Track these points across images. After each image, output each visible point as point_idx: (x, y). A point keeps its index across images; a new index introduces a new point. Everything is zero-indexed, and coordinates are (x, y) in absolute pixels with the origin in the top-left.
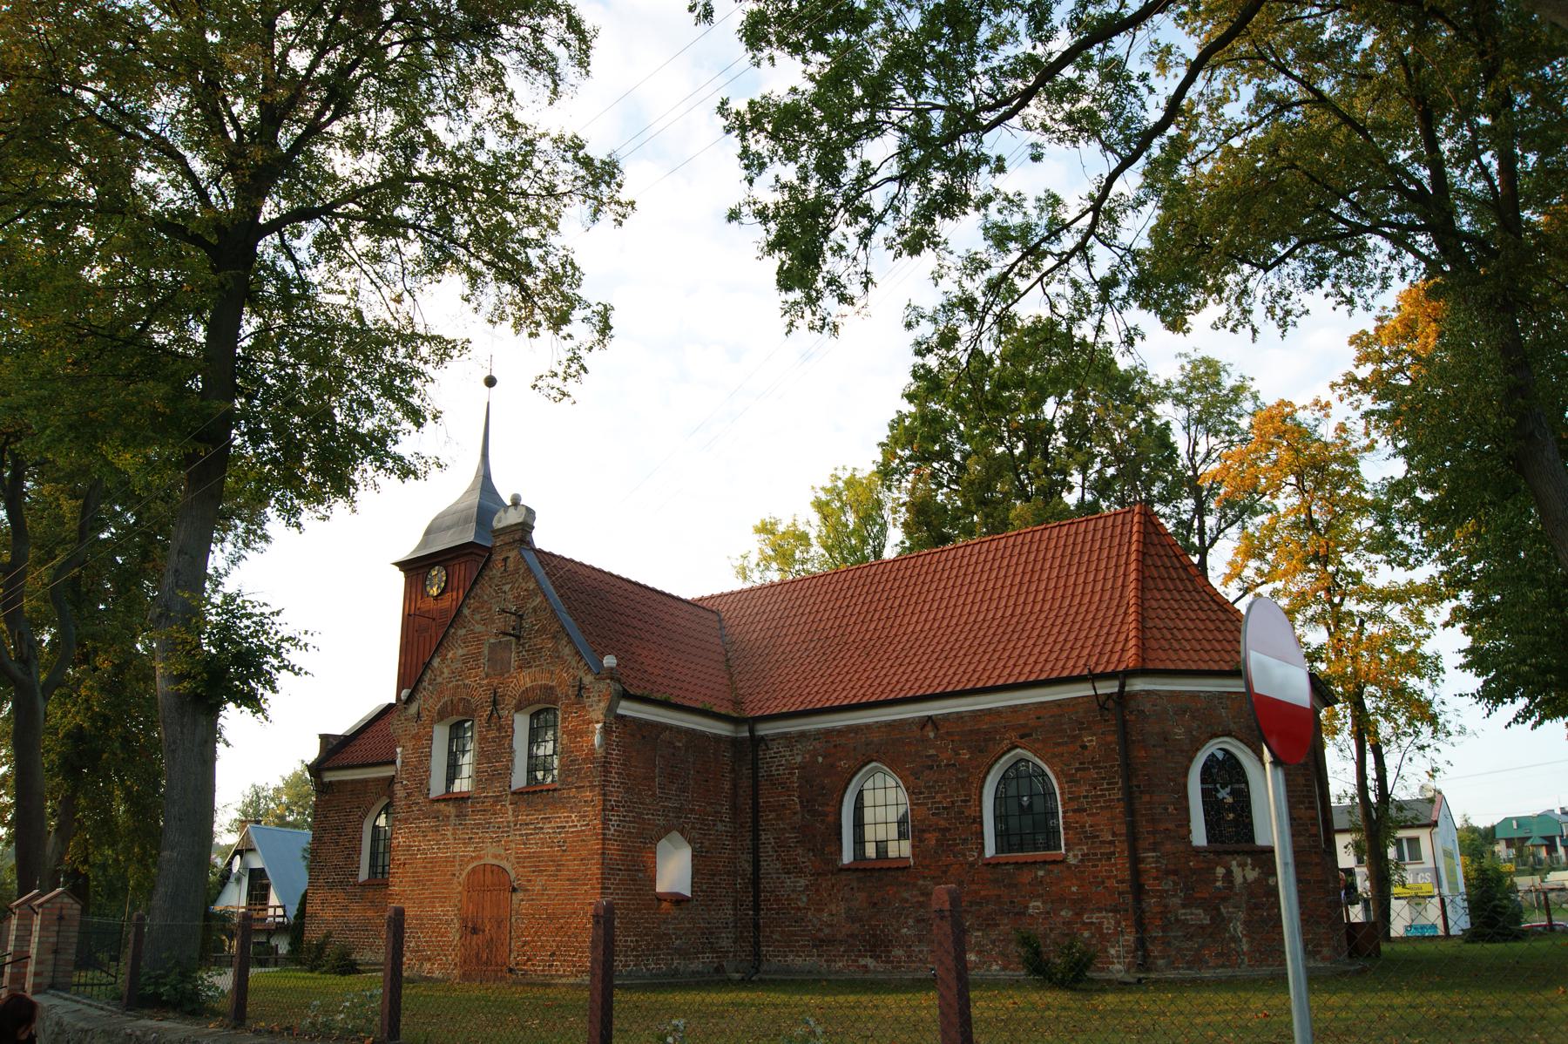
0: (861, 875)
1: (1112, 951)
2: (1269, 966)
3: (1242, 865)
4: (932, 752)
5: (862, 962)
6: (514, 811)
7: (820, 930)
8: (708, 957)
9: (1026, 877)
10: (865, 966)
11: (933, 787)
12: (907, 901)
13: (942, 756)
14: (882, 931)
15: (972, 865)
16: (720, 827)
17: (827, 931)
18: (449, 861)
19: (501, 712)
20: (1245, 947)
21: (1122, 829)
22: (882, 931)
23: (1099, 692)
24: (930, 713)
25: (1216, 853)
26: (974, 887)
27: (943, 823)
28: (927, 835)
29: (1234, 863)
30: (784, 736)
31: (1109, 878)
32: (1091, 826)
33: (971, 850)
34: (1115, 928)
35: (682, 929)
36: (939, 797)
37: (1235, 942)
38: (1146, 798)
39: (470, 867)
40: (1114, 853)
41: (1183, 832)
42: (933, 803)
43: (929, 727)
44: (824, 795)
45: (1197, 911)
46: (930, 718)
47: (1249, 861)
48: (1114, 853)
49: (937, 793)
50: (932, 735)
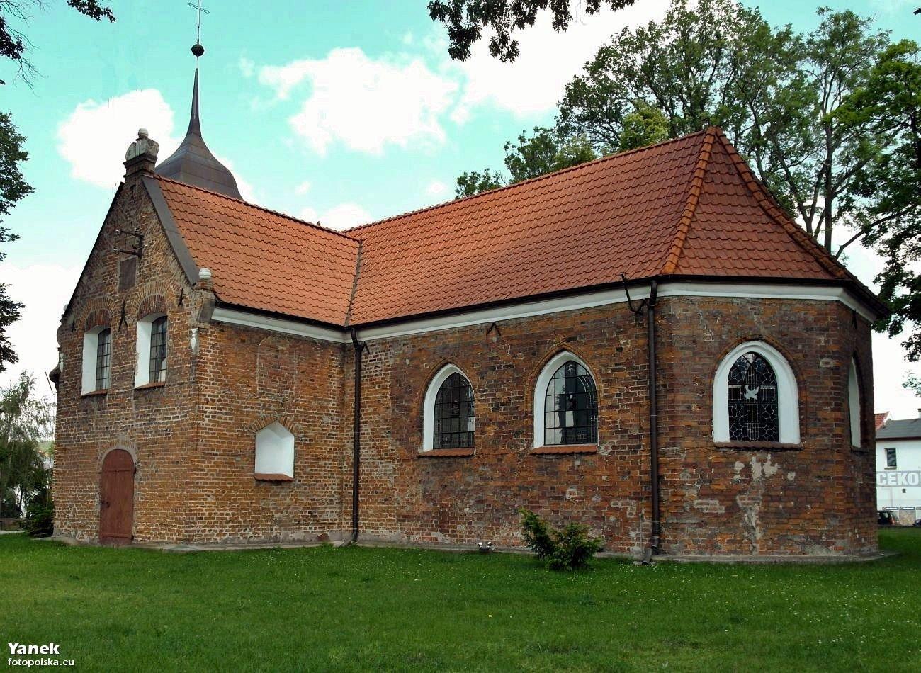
0: (435, 461)
1: (633, 534)
2: (780, 553)
3: (762, 461)
4: (495, 354)
5: (434, 534)
6: (137, 405)
7: (403, 507)
8: (311, 527)
9: (565, 466)
10: (436, 539)
11: (494, 386)
12: (469, 484)
13: (503, 358)
14: (450, 509)
15: (522, 454)
16: (326, 419)
17: (408, 508)
18: (94, 446)
19: (127, 321)
20: (758, 535)
21: (645, 424)
22: (450, 509)
23: (632, 298)
24: (494, 320)
25: (737, 449)
26: (524, 474)
27: (501, 418)
28: (487, 428)
29: (754, 458)
30: (382, 342)
31: (634, 469)
32: (622, 422)
33: (522, 441)
34: (637, 514)
35: (283, 504)
36: (499, 395)
37: (749, 531)
38: (670, 397)
39: (107, 452)
40: (639, 447)
41: (705, 428)
42: (494, 400)
43: (493, 332)
44: (410, 393)
45: (713, 502)
46: (494, 324)
47: (769, 457)
48: (639, 447)
49: (497, 391)
50: (495, 339)
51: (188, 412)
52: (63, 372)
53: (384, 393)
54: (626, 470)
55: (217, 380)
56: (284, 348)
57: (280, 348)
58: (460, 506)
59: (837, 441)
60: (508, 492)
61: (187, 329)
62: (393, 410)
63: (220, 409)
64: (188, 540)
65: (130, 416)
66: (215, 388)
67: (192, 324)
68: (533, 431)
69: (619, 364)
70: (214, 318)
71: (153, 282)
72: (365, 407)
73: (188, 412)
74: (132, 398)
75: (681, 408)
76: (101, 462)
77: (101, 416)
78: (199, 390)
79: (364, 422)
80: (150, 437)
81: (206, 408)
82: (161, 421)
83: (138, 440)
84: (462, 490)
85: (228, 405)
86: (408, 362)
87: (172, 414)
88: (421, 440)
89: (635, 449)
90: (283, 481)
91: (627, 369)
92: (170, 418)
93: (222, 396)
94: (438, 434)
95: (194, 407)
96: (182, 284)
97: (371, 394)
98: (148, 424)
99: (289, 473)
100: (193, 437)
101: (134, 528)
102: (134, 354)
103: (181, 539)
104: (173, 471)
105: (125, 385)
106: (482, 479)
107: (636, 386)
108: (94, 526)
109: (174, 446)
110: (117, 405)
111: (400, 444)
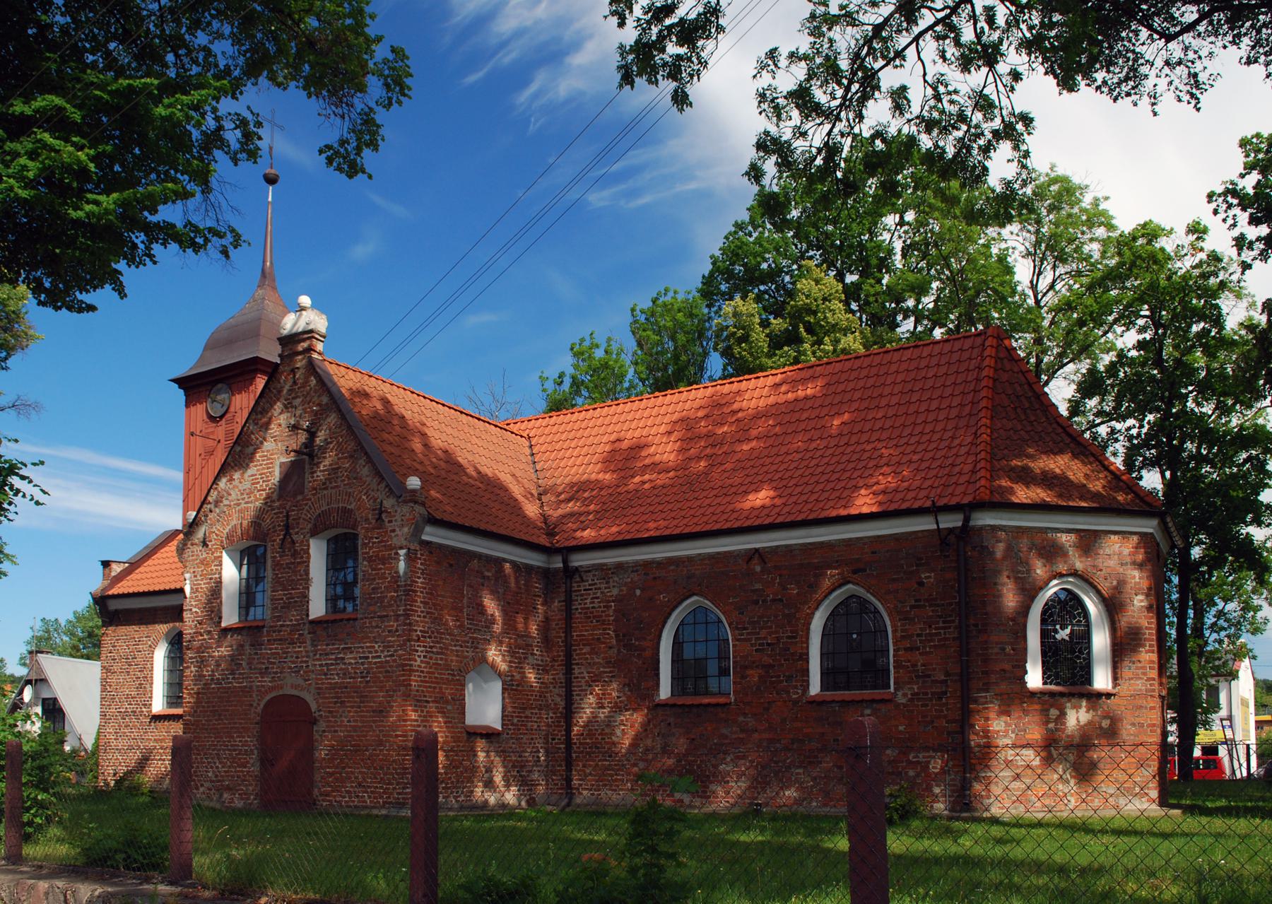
4: (758, 586)
12: (726, 737)
15: (795, 702)
18: (246, 691)
22: (699, 767)
24: (757, 546)
28: (750, 672)
30: (601, 567)
32: (923, 665)
33: (796, 687)
36: (763, 633)
39: (268, 698)
43: (755, 561)
46: (757, 550)
47: (1084, 704)
49: (762, 628)
50: (758, 569)
51: (396, 651)
52: (191, 598)
53: (604, 629)
54: (929, 719)
55: (428, 613)
56: (490, 574)
57: (487, 574)
58: (714, 762)
59: (1151, 685)
60: (778, 745)
61: (391, 550)
62: (619, 650)
63: (431, 647)
64: (400, 803)
65: (304, 654)
66: (427, 623)
67: (399, 544)
68: (808, 676)
69: (920, 600)
70: (424, 537)
71: (334, 491)
72: (578, 645)
73: (396, 651)
74: (306, 632)
75: (996, 650)
76: (259, 710)
77: (256, 654)
78: (410, 624)
79: (577, 664)
80: (337, 679)
81: (419, 646)
82: (353, 661)
83: (317, 684)
84: (715, 744)
85: (438, 642)
86: (638, 592)
87: (370, 652)
88: (658, 685)
89: (940, 696)
90: (493, 734)
91: (930, 606)
92: (368, 658)
93: (433, 632)
94: (676, 678)
95: (405, 645)
96: (381, 495)
97: (586, 631)
98: (332, 664)
99: (498, 726)
100: (404, 680)
101: (316, 790)
102: (306, 580)
103: (391, 803)
104: (374, 722)
105: (293, 616)
106: (742, 731)
107: (941, 625)
108: (251, 788)
109: (376, 692)
110: (280, 640)
111: (629, 690)
